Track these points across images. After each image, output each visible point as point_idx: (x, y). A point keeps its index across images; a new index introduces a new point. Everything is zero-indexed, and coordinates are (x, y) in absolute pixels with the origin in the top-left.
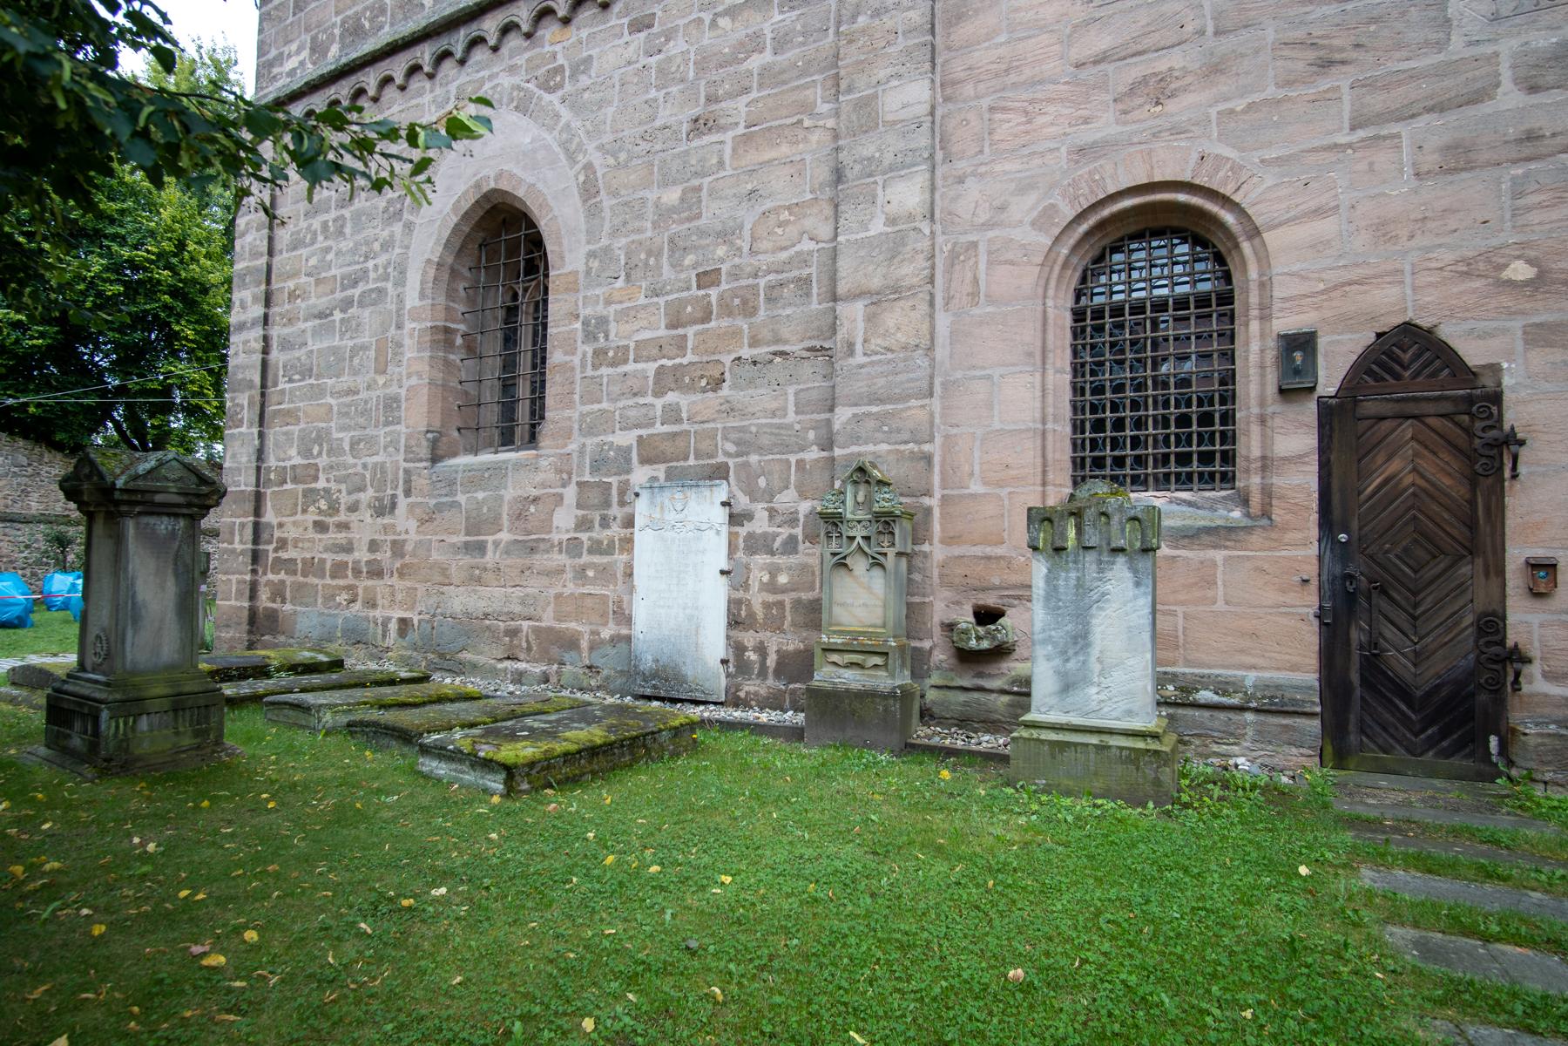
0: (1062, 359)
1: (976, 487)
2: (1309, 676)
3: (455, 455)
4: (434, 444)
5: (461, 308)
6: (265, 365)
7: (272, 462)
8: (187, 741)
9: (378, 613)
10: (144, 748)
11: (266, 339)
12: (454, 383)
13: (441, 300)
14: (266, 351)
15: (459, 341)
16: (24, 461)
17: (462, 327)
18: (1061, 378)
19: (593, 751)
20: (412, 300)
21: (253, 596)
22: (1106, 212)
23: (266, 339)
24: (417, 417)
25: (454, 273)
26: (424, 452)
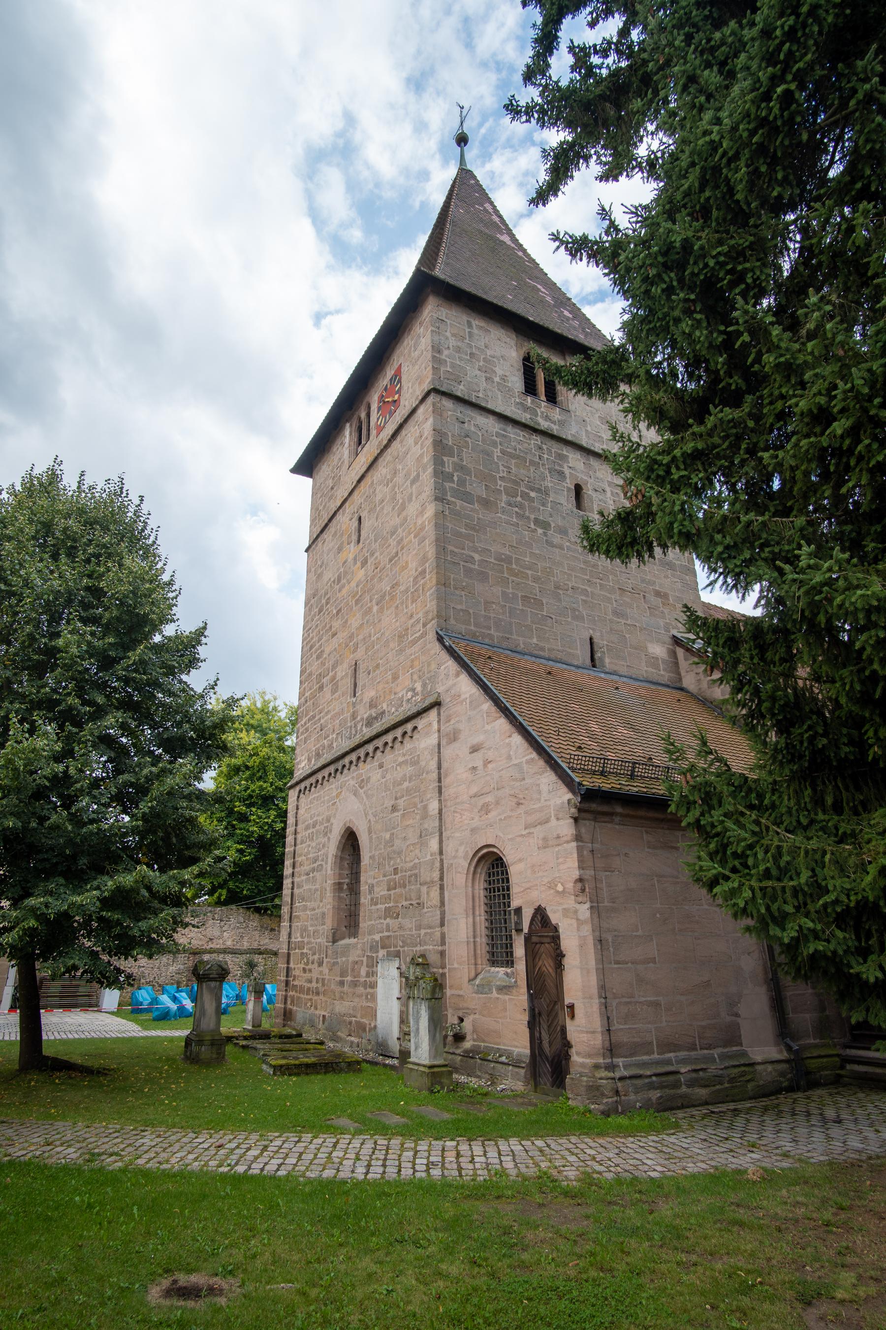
0: (481, 910)
1: (456, 966)
2: (528, 1051)
3: (344, 938)
4: (334, 934)
5: (346, 872)
6: (292, 894)
7: (293, 940)
8: (214, 1056)
9: (317, 1012)
10: (202, 1056)
11: (293, 883)
12: (343, 906)
13: (337, 871)
14: (293, 889)
15: (345, 887)
16: (242, 920)
17: (347, 881)
18: (481, 918)
19: (307, 1066)
20: (329, 872)
21: (285, 1003)
22: (480, 854)
23: (293, 883)
24: (329, 924)
25: (342, 859)
26: (331, 939)
